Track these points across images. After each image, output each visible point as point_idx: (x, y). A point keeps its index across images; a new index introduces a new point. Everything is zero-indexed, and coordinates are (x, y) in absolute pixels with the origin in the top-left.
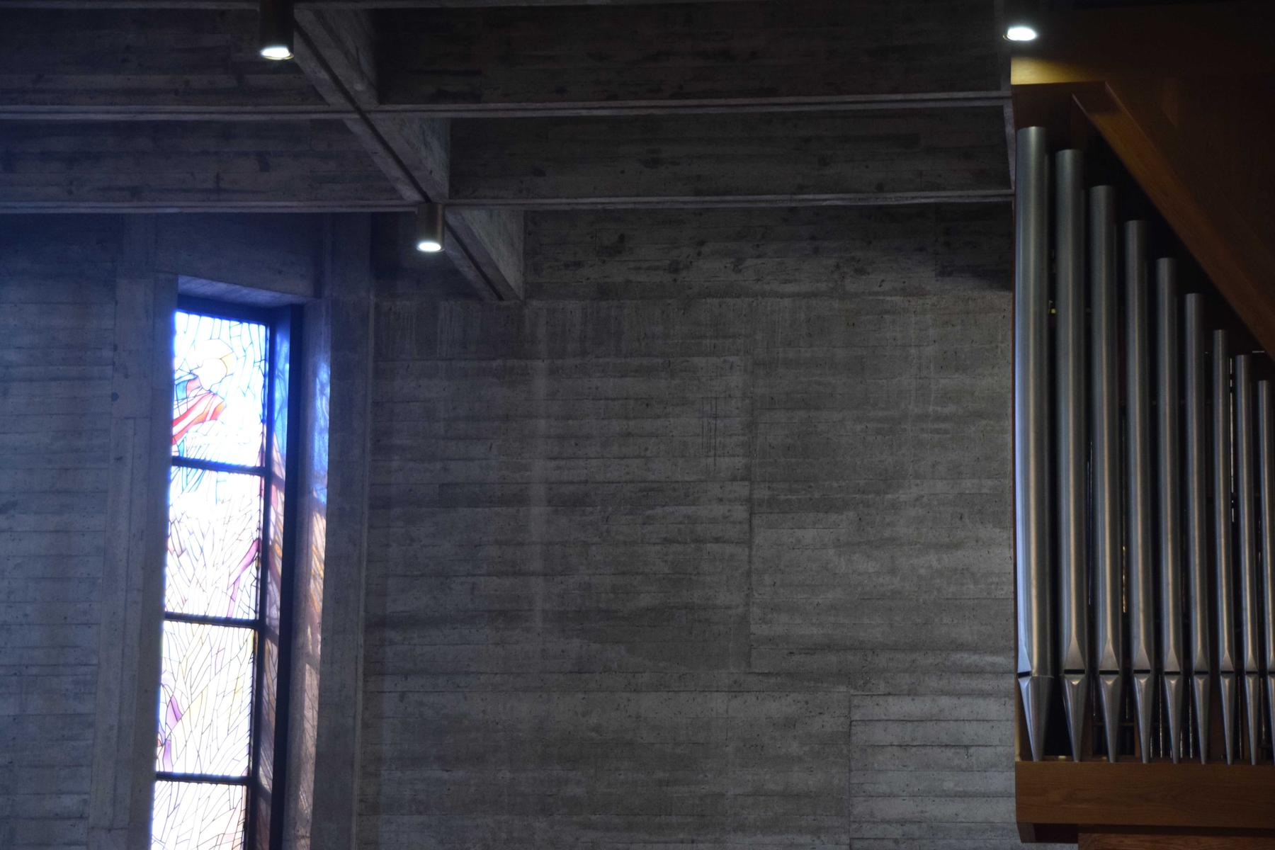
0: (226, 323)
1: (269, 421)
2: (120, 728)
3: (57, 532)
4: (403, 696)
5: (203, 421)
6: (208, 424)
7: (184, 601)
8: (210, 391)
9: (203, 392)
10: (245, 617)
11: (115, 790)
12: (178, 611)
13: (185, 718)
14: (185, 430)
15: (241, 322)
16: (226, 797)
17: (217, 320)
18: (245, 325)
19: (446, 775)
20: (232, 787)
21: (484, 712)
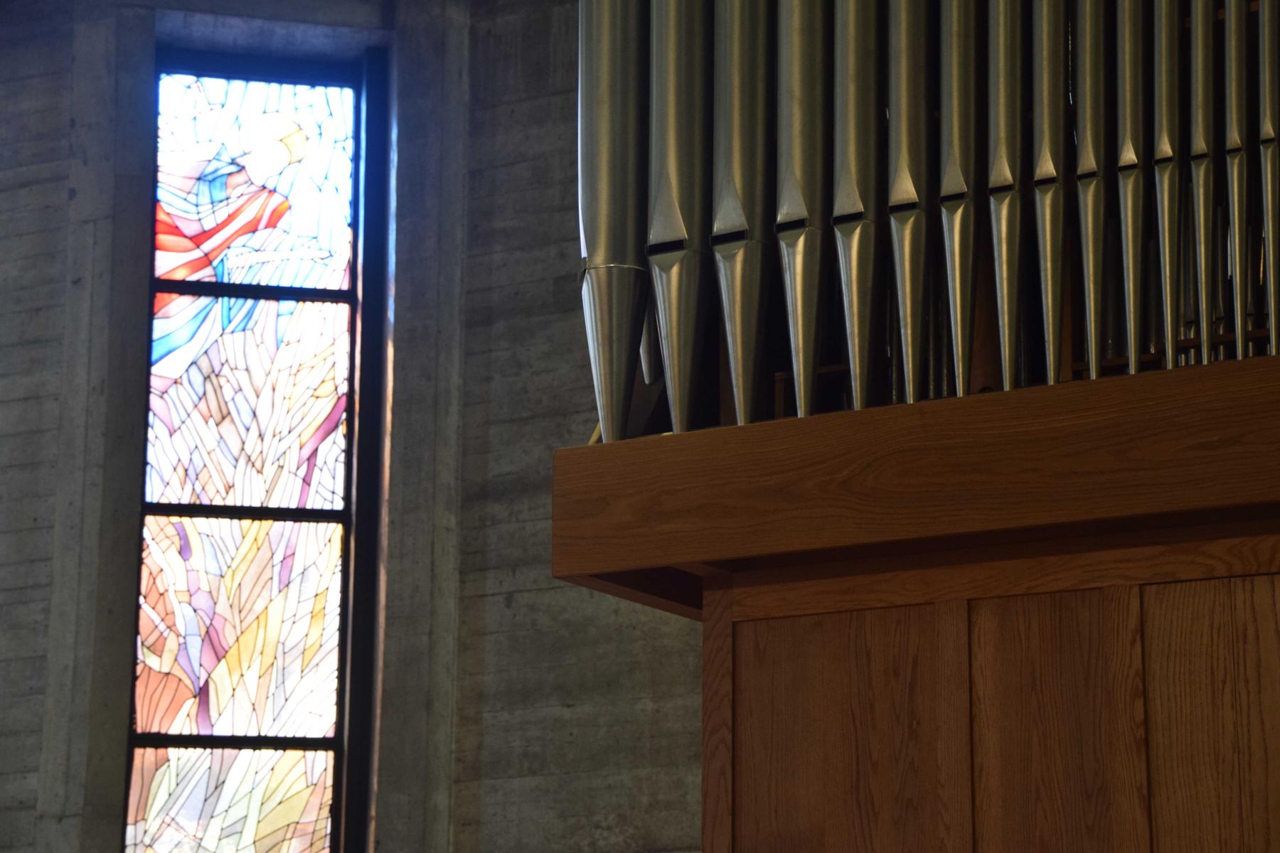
0: (288, 88)
1: (354, 225)
2: (75, 668)
3: (26, 399)
4: (509, 598)
5: (254, 231)
6: (262, 234)
7: (229, 488)
8: (264, 187)
9: (253, 188)
10: (327, 507)
11: (68, 759)
12: (218, 502)
13: (233, 653)
14: (226, 245)
15: (313, 85)
16: (300, 768)
17: (274, 86)
18: (320, 90)
19: (567, 713)
20: (310, 754)
21: (616, 612)
